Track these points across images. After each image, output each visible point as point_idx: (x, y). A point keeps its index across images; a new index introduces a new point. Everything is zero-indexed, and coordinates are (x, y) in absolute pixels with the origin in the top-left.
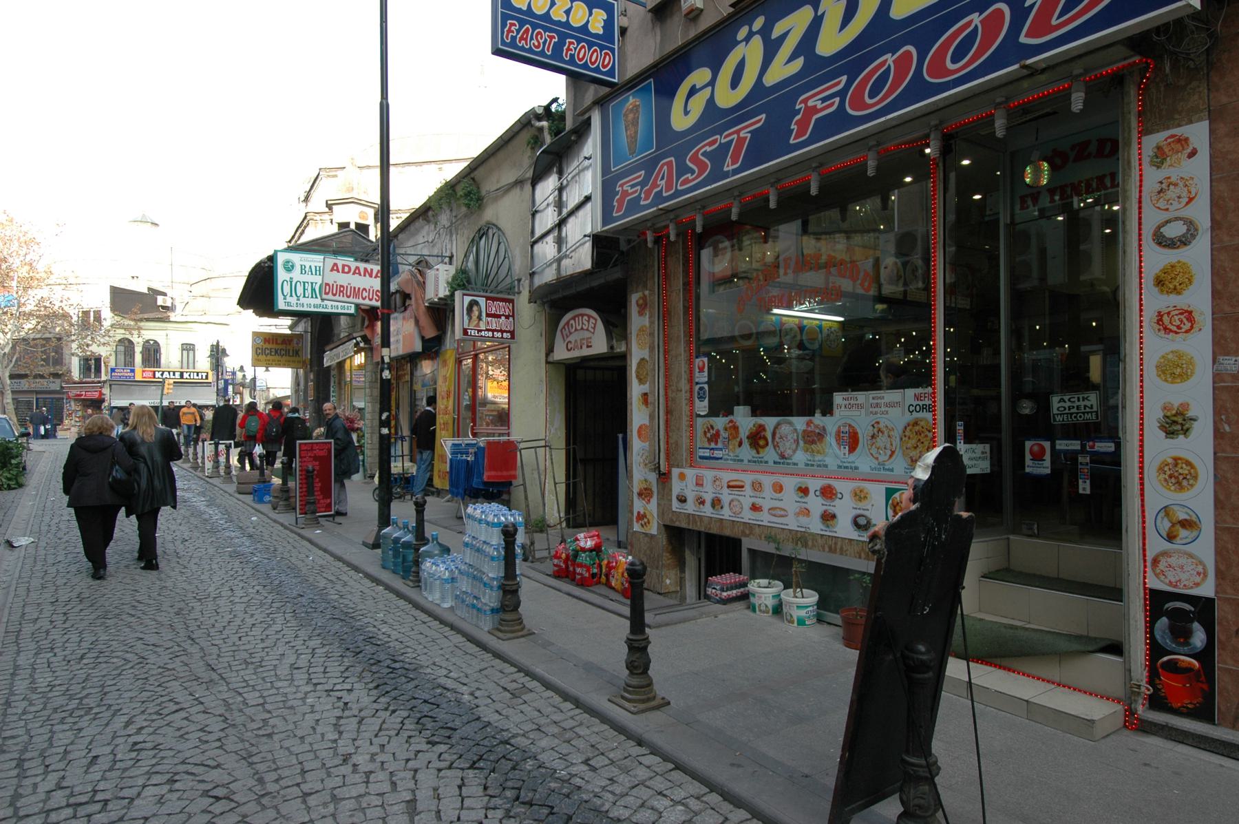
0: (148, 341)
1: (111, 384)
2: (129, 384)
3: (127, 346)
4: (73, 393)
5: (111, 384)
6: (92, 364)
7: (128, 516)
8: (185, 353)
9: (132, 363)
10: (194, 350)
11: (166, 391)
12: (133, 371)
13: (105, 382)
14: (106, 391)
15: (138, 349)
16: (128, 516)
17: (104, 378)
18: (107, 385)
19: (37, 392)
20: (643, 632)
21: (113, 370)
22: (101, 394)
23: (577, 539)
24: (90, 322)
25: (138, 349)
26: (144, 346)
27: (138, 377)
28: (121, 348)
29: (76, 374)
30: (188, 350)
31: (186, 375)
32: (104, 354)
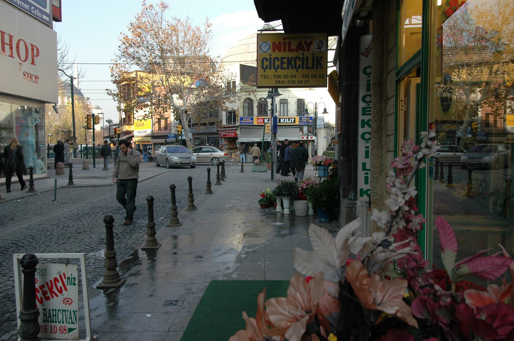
0: (260, 99)
1: (241, 127)
2: (249, 127)
3: (249, 102)
4: (223, 133)
5: (241, 127)
6: (232, 115)
7: (486, 290)
8: (282, 105)
9: (252, 114)
10: (287, 103)
11: (266, 131)
12: (252, 119)
13: (237, 127)
14: (238, 132)
15: (255, 104)
16: (486, 290)
17: (237, 124)
18: (239, 129)
19: (208, 134)
20: (153, 221)
21: (241, 119)
22: (236, 134)
23: (459, 139)
24: (230, 87)
25: (255, 104)
26: (258, 103)
27: (255, 123)
28: (246, 105)
29: (224, 123)
30: (284, 104)
31: (282, 121)
32: (236, 108)
